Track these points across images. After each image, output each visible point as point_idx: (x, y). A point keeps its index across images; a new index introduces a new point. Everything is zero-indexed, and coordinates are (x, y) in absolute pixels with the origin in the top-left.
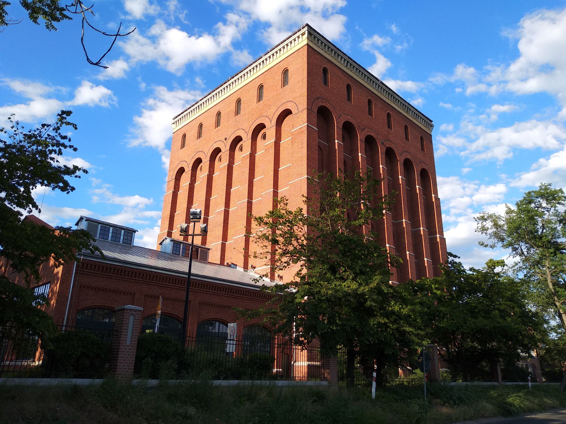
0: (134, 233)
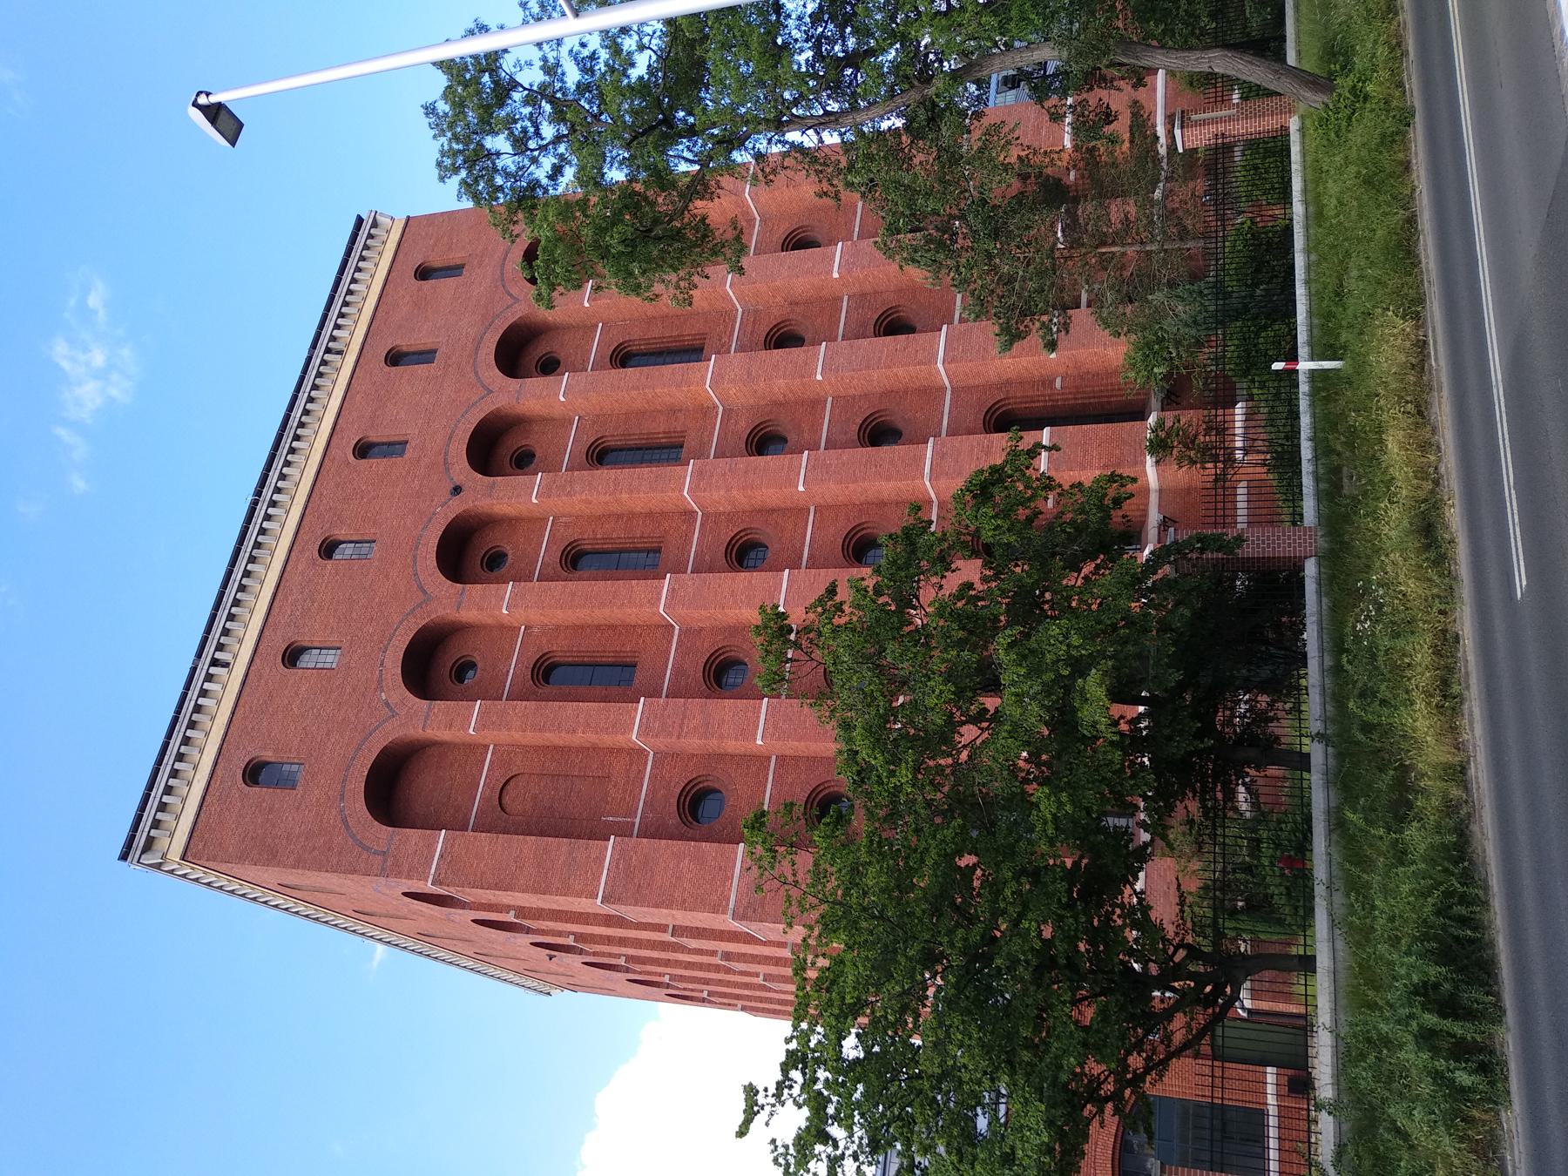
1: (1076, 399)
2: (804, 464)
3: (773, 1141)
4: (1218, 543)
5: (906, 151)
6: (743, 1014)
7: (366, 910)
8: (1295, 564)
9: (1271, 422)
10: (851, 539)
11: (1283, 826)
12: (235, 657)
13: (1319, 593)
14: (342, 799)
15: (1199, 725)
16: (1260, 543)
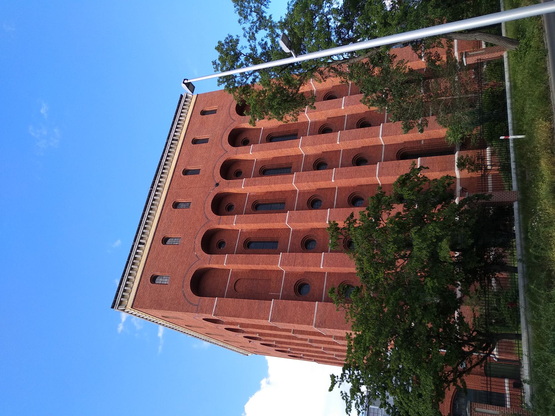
1: (429, 147)
2: (334, 173)
3: (341, 392)
4: (484, 197)
5: (371, 70)
6: (315, 363)
7: (190, 325)
8: (510, 204)
9: (500, 154)
10: (351, 197)
11: (508, 294)
12: (147, 241)
13: (519, 213)
14: (183, 287)
15: (480, 259)
16: (497, 197)
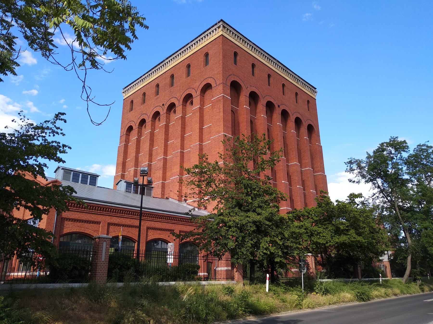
0: (97, 177)
14: (233, 75)
